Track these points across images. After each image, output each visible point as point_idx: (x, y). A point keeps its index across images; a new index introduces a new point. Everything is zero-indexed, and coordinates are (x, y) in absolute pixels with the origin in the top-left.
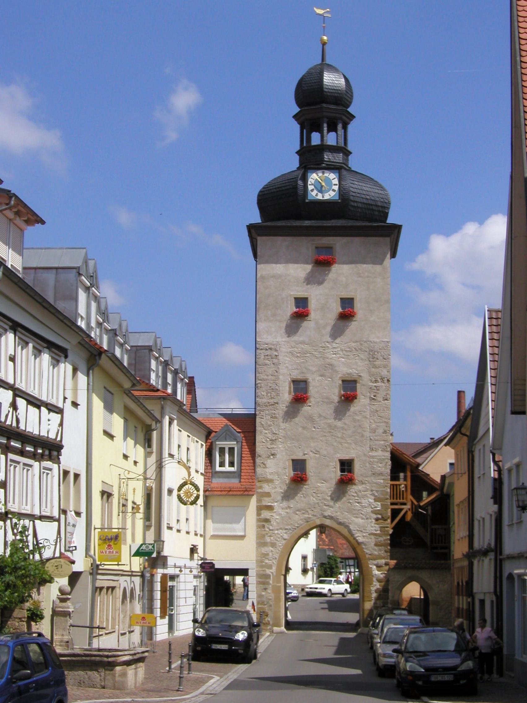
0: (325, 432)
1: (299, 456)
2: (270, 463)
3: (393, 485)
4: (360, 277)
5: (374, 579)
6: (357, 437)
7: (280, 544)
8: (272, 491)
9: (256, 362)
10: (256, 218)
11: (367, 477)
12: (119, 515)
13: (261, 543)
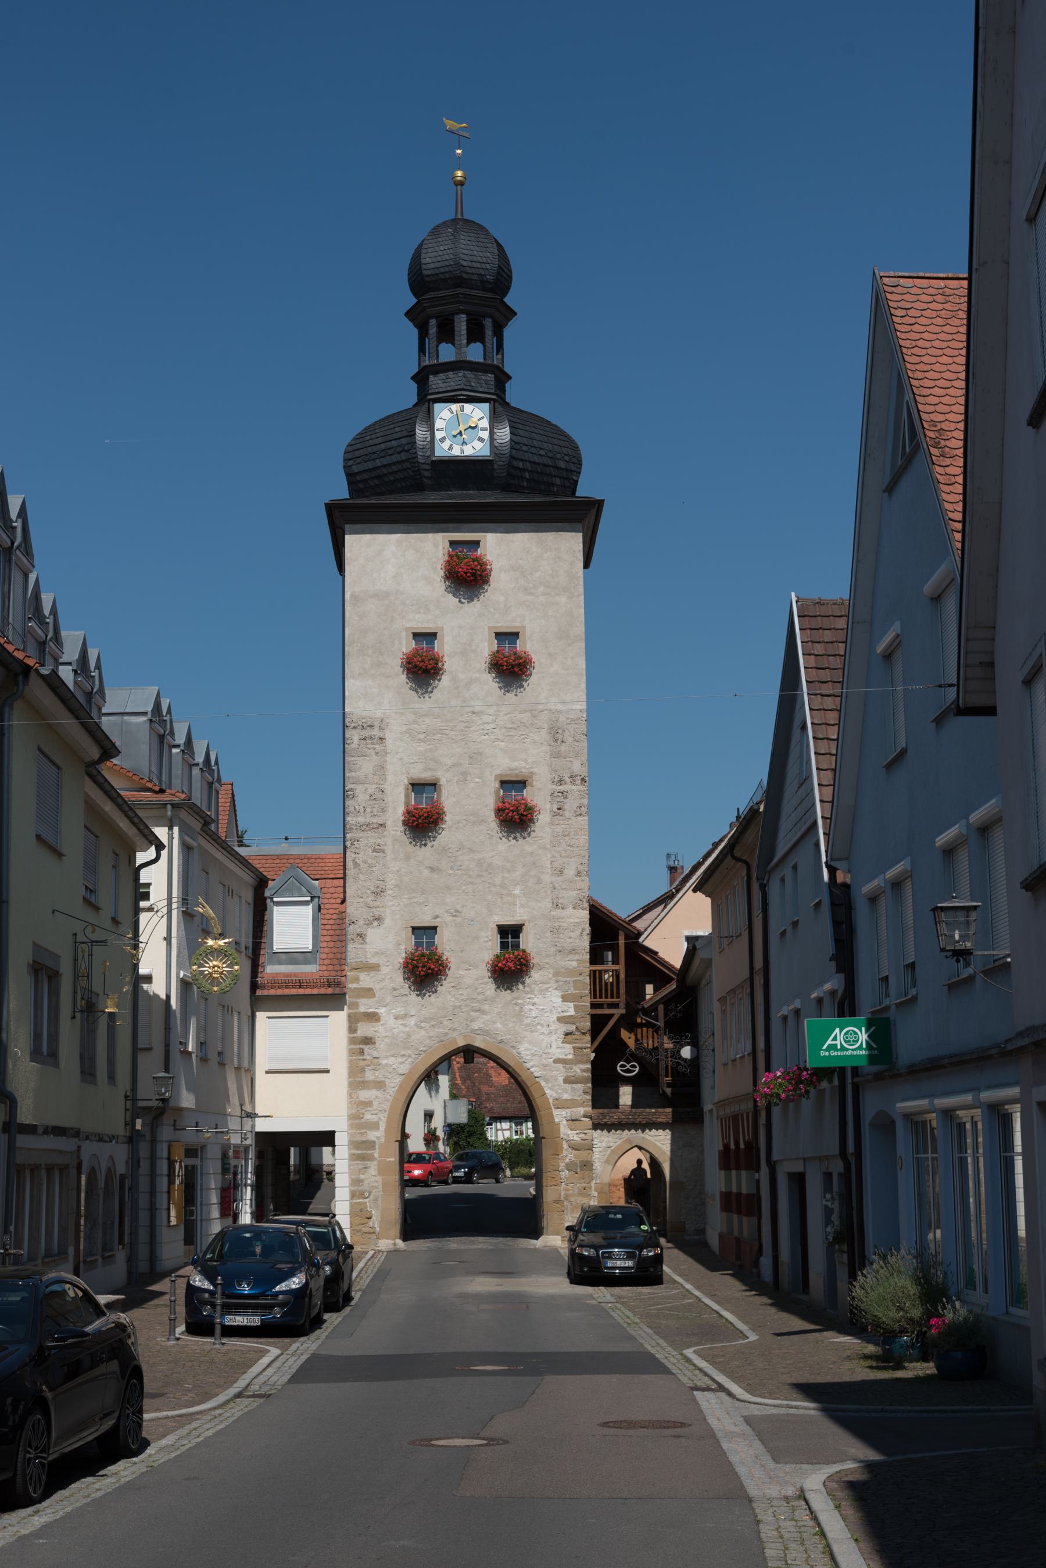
0: (470, 877)
3: (594, 971)
4: (531, 594)
5: (565, 1146)
6: (529, 884)
7: (394, 1083)
8: (376, 987)
10: (341, 491)
11: (548, 956)
12: (74, 1017)
13: (357, 1081)
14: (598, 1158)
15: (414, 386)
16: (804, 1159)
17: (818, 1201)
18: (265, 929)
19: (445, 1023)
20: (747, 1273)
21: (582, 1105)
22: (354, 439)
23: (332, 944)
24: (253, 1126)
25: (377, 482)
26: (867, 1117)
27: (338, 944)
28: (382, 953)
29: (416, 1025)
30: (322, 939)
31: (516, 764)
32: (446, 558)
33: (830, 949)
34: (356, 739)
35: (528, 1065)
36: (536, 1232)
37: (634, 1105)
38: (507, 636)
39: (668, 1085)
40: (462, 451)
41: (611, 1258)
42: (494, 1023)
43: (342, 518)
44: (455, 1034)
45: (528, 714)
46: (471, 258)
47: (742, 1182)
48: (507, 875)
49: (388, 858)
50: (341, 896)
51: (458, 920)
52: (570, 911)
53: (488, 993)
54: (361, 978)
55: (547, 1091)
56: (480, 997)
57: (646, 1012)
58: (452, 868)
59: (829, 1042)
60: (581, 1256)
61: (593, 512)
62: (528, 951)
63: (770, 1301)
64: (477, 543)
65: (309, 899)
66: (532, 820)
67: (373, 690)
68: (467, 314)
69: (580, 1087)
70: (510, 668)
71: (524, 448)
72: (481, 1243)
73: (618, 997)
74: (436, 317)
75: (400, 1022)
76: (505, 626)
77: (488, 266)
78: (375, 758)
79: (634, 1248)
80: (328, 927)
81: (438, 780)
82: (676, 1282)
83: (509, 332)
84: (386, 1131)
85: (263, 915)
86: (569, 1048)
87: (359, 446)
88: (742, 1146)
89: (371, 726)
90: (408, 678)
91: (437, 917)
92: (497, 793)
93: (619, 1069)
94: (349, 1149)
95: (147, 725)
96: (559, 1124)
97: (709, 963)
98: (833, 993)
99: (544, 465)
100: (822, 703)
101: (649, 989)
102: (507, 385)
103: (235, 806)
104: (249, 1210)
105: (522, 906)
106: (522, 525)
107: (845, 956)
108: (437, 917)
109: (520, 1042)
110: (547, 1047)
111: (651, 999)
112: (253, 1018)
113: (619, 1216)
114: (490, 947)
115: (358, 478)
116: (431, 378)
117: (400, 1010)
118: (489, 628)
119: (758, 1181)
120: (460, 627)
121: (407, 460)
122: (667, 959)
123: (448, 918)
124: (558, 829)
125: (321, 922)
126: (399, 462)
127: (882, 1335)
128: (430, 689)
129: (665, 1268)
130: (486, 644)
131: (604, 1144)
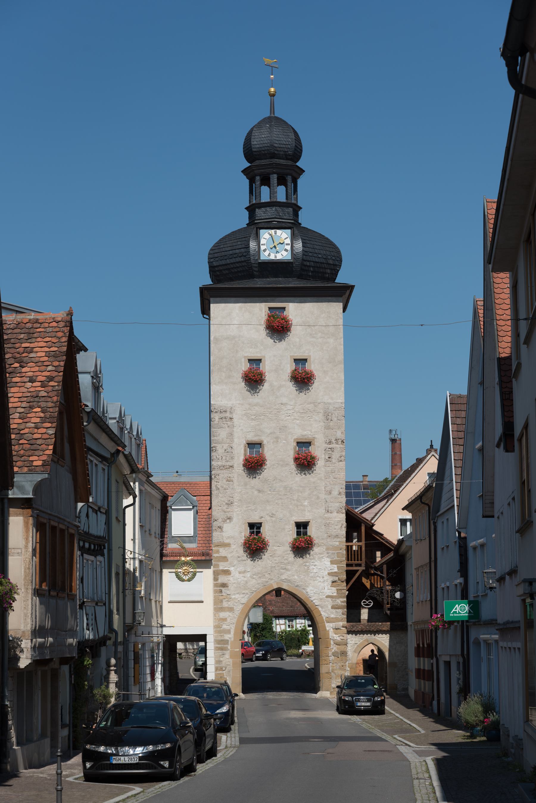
0: (280, 495)
1: (255, 519)
2: (227, 527)
5: (332, 643)
6: (313, 500)
7: (238, 608)
8: (229, 556)
9: (210, 425)
10: (208, 281)
11: (323, 539)
13: (218, 607)
14: (350, 650)
15: (247, 213)
16: (450, 655)
17: (455, 674)
18: (167, 523)
19: (267, 576)
20: (426, 711)
21: (341, 621)
22: (214, 246)
23: (204, 532)
24: (162, 632)
25: (227, 272)
26: (472, 639)
27: (208, 532)
28: (232, 537)
29: (251, 577)
30: (199, 529)
31: (305, 432)
32: (267, 317)
33: (458, 567)
34: (217, 418)
35: (312, 599)
36: (315, 690)
37: (369, 620)
38: (300, 361)
39: (389, 609)
40: (276, 257)
41: (359, 701)
42: (293, 576)
43: (207, 297)
44: (272, 582)
45: (312, 405)
46: (280, 142)
47: (426, 664)
48: (300, 494)
49: (235, 485)
50: (209, 505)
51: (274, 519)
52: (335, 514)
53: (290, 559)
54: (221, 551)
55: (323, 613)
56: (286, 562)
57: (376, 569)
58: (270, 490)
59: (454, 610)
60: (344, 700)
61: (348, 292)
62: (312, 536)
63: (432, 720)
64: (284, 309)
65: (191, 507)
66: (314, 464)
67: (227, 391)
68: (277, 174)
69: (340, 611)
70: (302, 379)
71: (310, 254)
72: (285, 696)
73: (361, 560)
74: (260, 175)
75: (242, 575)
76: (299, 356)
77: (289, 146)
78: (227, 429)
79: (371, 696)
80: (202, 523)
81: (263, 441)
82: (391, 713)
83: (300, 182)
84: (234, 634)
85: (166, 516)
86: (334, 589)
87: (217, 251)
88: (426, 646)
89: (225, 411)
90: (245, 384)
91: (262, 517)
92: (295, 448)
93: (362, 604)
94: (214, 644)
95: (116, 424)
96: (329, 631)
97: (410, 547)
98: (461, 584)
99: (321, 263)
100: (459, 449)
101: (378, 554)
102: (300, 213)
103: (147, 455)
104: (160, 677)
105: (309, 511)
106: (309, 299)
107: (464, 570)
108: (262, 517)
109: (307, 586)
110: (322, 589)
111: (380, 561)
112: (161, 572)
113: (363, 681)
114: (291, 534)
115: (216, 269)
116: (257, 210)
117: (242, 569)
118: (291, 356)
119: (432, 664)
120: (274, 356)
121: (245, 261)
122: (388, 538)
123: (268, 518)
124: (329, 469)
125: (197, 520)
126: (240, 262)
127: (467, 727)
128: (258, 391)
129: (386, 707)
130: (289, 366)
131: (353, 642)
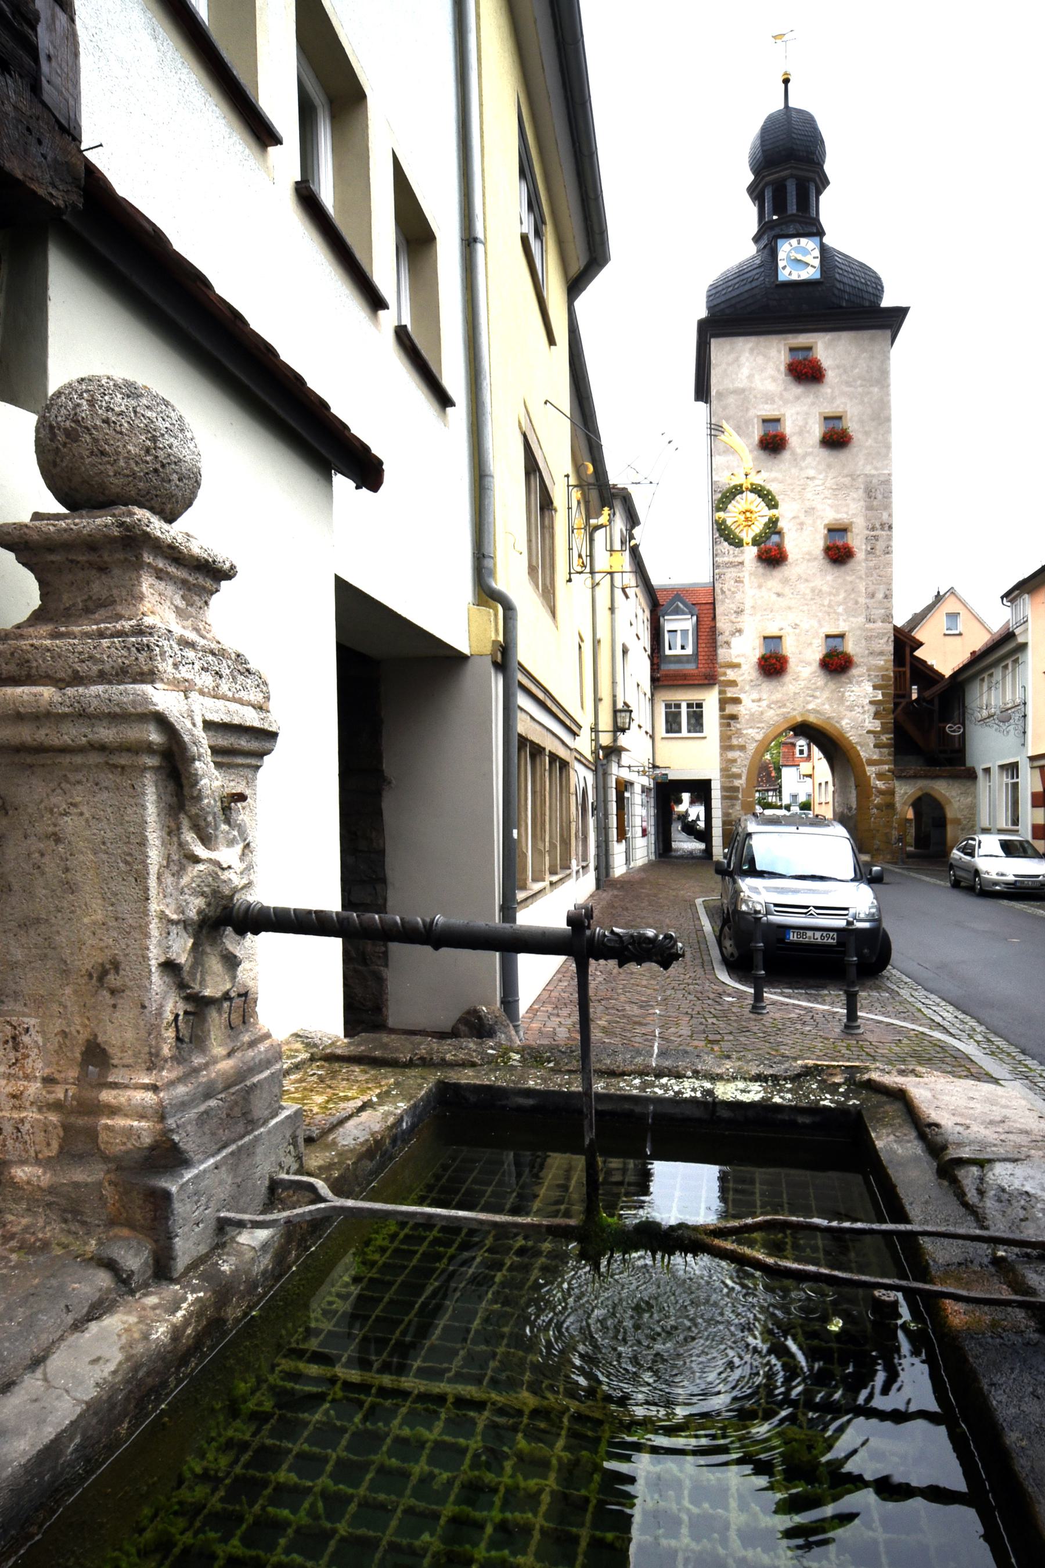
4: (851, 386)
8: (739, 679)
13: (726, 745)
